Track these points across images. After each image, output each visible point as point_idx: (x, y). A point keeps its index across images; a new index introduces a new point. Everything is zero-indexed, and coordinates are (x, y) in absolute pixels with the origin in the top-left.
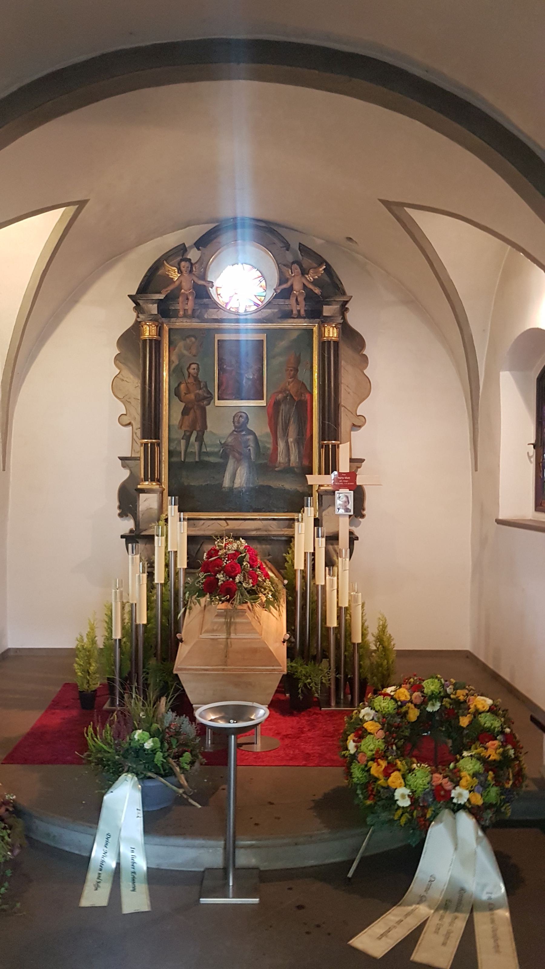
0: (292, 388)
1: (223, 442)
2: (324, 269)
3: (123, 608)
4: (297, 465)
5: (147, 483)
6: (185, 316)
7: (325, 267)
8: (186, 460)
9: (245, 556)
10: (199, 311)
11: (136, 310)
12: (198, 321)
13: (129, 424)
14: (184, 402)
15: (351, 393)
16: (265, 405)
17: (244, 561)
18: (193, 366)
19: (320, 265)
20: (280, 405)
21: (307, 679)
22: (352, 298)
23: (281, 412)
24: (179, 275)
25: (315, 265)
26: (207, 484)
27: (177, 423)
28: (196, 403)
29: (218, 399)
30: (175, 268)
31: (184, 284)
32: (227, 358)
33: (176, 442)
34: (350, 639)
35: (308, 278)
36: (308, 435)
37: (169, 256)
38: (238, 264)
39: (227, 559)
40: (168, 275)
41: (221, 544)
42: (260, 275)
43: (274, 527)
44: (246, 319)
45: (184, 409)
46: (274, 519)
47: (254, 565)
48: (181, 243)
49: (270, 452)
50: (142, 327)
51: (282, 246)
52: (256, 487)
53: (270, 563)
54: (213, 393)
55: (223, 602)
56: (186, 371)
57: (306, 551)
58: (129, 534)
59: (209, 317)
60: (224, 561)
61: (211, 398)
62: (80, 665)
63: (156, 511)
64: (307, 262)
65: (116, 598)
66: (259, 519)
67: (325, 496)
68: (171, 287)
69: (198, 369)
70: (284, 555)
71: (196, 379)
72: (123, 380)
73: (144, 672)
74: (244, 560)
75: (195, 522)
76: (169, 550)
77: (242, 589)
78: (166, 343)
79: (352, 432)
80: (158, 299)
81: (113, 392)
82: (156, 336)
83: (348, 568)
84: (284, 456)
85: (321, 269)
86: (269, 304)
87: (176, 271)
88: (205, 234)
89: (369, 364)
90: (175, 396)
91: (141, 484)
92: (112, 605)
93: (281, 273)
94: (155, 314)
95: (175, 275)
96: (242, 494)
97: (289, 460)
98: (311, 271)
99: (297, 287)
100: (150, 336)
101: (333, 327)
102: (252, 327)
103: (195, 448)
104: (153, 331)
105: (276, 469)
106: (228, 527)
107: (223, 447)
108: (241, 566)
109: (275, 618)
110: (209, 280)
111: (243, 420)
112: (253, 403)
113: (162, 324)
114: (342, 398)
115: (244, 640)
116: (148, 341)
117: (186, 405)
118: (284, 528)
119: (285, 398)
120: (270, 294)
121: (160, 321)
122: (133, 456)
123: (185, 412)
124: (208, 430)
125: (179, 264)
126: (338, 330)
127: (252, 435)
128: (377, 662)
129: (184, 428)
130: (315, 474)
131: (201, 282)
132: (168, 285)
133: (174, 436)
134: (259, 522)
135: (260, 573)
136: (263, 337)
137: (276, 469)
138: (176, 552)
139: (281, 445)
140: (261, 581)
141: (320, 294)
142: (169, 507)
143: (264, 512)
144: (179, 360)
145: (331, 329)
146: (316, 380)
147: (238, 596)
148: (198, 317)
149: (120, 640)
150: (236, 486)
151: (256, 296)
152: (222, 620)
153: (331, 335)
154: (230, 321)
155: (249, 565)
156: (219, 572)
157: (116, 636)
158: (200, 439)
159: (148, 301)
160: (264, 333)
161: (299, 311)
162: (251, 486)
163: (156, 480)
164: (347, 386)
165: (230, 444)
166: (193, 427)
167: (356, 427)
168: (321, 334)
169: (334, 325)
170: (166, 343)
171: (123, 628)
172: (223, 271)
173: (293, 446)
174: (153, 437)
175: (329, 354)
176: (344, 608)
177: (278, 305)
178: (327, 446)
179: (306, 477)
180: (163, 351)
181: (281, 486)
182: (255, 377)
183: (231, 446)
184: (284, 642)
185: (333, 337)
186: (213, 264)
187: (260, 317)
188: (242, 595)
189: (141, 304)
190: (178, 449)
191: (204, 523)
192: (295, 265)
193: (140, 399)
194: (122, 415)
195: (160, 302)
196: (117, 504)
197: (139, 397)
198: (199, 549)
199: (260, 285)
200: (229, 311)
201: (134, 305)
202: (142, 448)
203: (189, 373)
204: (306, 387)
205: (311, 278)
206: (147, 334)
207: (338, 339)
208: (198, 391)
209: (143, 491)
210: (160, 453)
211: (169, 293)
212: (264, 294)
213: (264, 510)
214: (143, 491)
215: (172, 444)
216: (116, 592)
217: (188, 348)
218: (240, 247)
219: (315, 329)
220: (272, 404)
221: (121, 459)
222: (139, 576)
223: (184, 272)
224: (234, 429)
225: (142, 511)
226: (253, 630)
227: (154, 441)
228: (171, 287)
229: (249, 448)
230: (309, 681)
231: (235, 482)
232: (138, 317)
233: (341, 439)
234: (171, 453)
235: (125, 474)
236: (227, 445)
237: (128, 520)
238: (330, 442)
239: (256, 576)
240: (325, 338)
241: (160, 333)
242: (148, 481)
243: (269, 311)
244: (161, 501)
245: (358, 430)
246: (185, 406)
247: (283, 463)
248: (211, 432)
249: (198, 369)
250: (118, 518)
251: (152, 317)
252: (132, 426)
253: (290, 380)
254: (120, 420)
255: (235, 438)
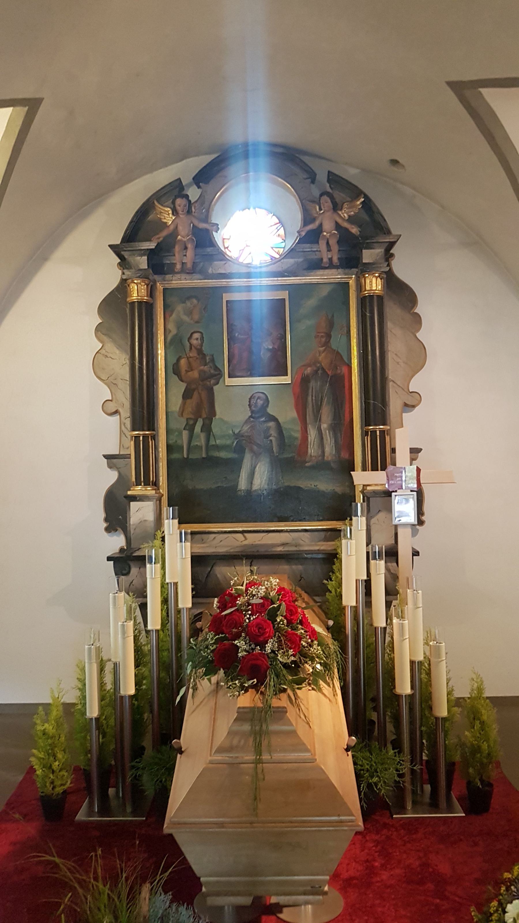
0: (324, 360)
1: (237, 431)
2: (362, 203)
3: (101, 670)
4: (334, 458)
5: (139, 488)
6: (184, 270)
7: (363, 200)
8: (190, 457)
9: (279, 606)
10: (202, 264)
11: (120, 265)
12: (201, 277)
13: (116, 412)
14: (186, 382)
15: (402, 364)
16: (290, 382)
17: (277, 615)
18: (196, 335)
19: (357, 197)
20: (309, 382)
21: (372, 777)
22: (402, 237)
23: (310, 391)
24: (173, 218)
25: (350, 199)
26: (218, 487)
27: (178, 409)
28: (201, 383)
29: (229, 377)
30: (169, 209)
31: (180, 228)
32: (239, 324)
33: (177, 433)
34: (431, 708)
35: (342, 215)
36: (347, 419)
37: (161, 197)
38: (249, 209)
39: (250, 612)
40: (161, 219)
41: (241, 587)
42: (278, 221)
43: (307, 541)
44: (260, 273)
45: (185, 391)
46: (306, 531)
47: (293, 619)
48: (176, 178)
49: (298, 442)
50: (129, 286)
51: (305, 177)
52: (280, 488)
53: (306, 594)
54: (222, 370)
55: (246, 691)
56: (187, 343)
57: (357, 578)
58: (413, 310)
59: (214, 272)
60: (245, 616)
61: (219, 376)
62: (39, 759)
63: (152, 525)
64: (339, 195)
65: (90, 658)
66: (287, 531)
67: (373, 498)
68: (164, 233)
69: (202, 338)
70: (325, 582)
71: (200, 351)
72: (106, 356)
73: (133, 767)
74: (278, 613)
75: (204, 536)
76: (167, 581)
77: (276, 664)
78: (160, 308)
79: (404, 414)
80: (148, 249)
81: (94, 373)
82: (147, 297)
83: (421, 605)
84: (315, 446)
85: (358, 203)
86: (291, 253)
87: (170, 212)
88: (207, 165)
89: (423, 325)
90: (173, 375)
91: (132, 489)
92: (84, 667)
93: (305, 211)
94: (145, 269)
95: (169, 218)
96: (263, 499)
97: (323, 452)
98: (345, 205)
99: (328, 226)
100: (139, 298)
101: (377, 277)
102: (270, 283)
103: (201, 440)
104: (143, 291)
105: (307, 465)
106: (246, 542)
107: (236, 439)
108: (273, 623)
109: (328, 700)
110: (213, 222)
111: (261, 402)
112: (274, 380)
113: (155, 282)
114: (390, 372)
115: (285, 766)
116: (136, 304)
117: (187, 385)
118: (320, 541)
119: (316, 372)
120: (290, 244)
121: (151, 277)
122: (121, 453)
123: (187, 395)
124: (217, 417)
125: (173, 203)
126: (383, 280)
127: (274, 421)
128: (472, 745)
129: (186, 416)
130: (357, 471)
131: (202, 226)
132: (161, 231)
133: (174, 425)
134: (287, 534)
135: (303, 631)
136: (285, 295)
137: (307, 465)
138: (176, 584)
139: (312, 434)
140: (306, 645)
141: (359, 233)
142: (166, 522)
143: (292, 521)
144: (178, 328)
145: (374, 280)
146: (355, 348)
147: (271, 680)
148: (200, 272)
149: (97, 719)
150: (255, 487)
151: (272, 248)
152: (247, 727)
153: (374, 288)
154: (240, 276)
155: (285, 621)
156: (237, 636)
157: (91, 713)
158: (207, 429)
159: (134, 252)
160: (286, 290)
161: (331, 259)
162: (274, 487)
163: (151, 484)
164: (396, 354)
165: (246, 434)
166: (197, 414)
167: (409, 407)
168: (360, 287)
169: (377, 275)
170: (160, 308)
171: (102, 698)
172: (231, 218)
173: (328, 434)
174: (145, 428)
175: (372, 313)
176: (418, 662)
177: (302, 253)
178: (374, 432)
179: (351, 474)
180: (157, 315)
181: (313, 486)
182: (276, 347)
183: (247, 436)
184: (347, 750)
185: (376, 290)
186: (218, 204)
187: (280, 269)
188: (277, 676)
189: (126, 257)
190: (179, 442)
191: (215, 538)
192: (325, 198)
193: (128, 380)
194: (107, 401)
195: (151, 254)
196: (103, 515)
197: (127, 377)
198: (210, 572)
199: (277, 234)
200: (241, 264)
201: (119, 261)
202: (132, 443)
203: (191, 345)
204: (341, 356)
205: (345, 215)
206: (135, 294)
207: (383, 293)
208: (202, 367)
209: (134, 498)
210: (156, 448)
211: (162, 242)
212: (283, 245)
213: (292, 518)
214: (134, 498)
215: (171, 437)
216: (90, 649)
217: (189, 313)
218: (251, 184)
219: (352, 282)
220: (299, 381)
221: (107, 457)
222: (123, 626)
223: (180, 212)
224: (250, 414)
225: (133, 525)
226: (301, 747)
227: (147, 433)
228: (164, 233)
229: (271, 438)
230: (375, 779)
231: (253, 483)
232: (123, 273)
233: (390, 423)
234: (170, 448)
235: (113, 476)
236: (243, 436)
237: (118, 536)
238: (378, 427)
239: (298, 639)
240: (366, 292)
241: (151, 293)
242: (141, 485)
243: (291, 261)
244: (158, 511)
245: (411, 411)
246: (187, 387)
247: (315, 457)
248: (222, 420)
249: (202, 338)
250: (105, 534)
251: (141, 272)
252: (120, 414)
253: (322, 349)
254: (105, 408)
255: (252, 427)
